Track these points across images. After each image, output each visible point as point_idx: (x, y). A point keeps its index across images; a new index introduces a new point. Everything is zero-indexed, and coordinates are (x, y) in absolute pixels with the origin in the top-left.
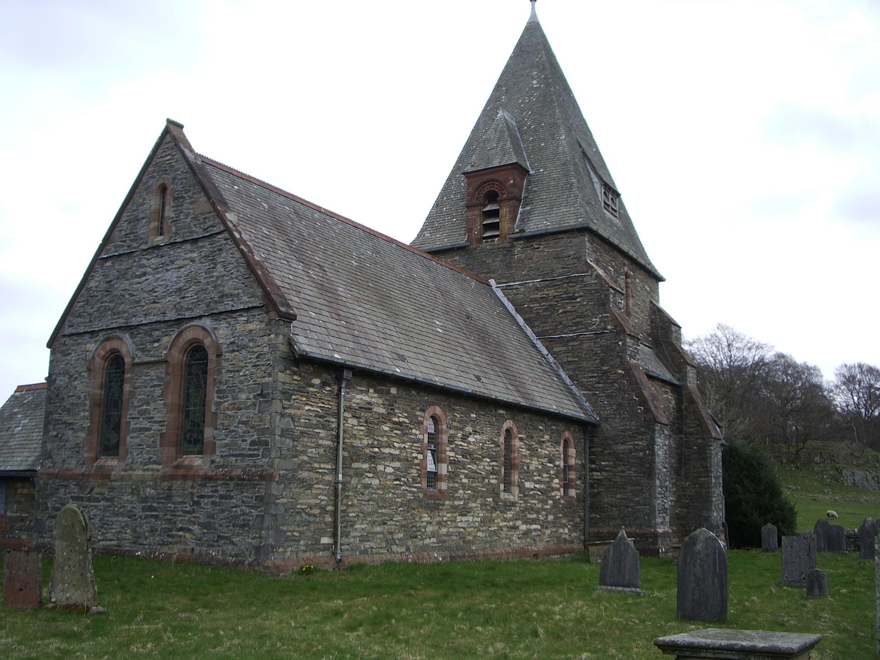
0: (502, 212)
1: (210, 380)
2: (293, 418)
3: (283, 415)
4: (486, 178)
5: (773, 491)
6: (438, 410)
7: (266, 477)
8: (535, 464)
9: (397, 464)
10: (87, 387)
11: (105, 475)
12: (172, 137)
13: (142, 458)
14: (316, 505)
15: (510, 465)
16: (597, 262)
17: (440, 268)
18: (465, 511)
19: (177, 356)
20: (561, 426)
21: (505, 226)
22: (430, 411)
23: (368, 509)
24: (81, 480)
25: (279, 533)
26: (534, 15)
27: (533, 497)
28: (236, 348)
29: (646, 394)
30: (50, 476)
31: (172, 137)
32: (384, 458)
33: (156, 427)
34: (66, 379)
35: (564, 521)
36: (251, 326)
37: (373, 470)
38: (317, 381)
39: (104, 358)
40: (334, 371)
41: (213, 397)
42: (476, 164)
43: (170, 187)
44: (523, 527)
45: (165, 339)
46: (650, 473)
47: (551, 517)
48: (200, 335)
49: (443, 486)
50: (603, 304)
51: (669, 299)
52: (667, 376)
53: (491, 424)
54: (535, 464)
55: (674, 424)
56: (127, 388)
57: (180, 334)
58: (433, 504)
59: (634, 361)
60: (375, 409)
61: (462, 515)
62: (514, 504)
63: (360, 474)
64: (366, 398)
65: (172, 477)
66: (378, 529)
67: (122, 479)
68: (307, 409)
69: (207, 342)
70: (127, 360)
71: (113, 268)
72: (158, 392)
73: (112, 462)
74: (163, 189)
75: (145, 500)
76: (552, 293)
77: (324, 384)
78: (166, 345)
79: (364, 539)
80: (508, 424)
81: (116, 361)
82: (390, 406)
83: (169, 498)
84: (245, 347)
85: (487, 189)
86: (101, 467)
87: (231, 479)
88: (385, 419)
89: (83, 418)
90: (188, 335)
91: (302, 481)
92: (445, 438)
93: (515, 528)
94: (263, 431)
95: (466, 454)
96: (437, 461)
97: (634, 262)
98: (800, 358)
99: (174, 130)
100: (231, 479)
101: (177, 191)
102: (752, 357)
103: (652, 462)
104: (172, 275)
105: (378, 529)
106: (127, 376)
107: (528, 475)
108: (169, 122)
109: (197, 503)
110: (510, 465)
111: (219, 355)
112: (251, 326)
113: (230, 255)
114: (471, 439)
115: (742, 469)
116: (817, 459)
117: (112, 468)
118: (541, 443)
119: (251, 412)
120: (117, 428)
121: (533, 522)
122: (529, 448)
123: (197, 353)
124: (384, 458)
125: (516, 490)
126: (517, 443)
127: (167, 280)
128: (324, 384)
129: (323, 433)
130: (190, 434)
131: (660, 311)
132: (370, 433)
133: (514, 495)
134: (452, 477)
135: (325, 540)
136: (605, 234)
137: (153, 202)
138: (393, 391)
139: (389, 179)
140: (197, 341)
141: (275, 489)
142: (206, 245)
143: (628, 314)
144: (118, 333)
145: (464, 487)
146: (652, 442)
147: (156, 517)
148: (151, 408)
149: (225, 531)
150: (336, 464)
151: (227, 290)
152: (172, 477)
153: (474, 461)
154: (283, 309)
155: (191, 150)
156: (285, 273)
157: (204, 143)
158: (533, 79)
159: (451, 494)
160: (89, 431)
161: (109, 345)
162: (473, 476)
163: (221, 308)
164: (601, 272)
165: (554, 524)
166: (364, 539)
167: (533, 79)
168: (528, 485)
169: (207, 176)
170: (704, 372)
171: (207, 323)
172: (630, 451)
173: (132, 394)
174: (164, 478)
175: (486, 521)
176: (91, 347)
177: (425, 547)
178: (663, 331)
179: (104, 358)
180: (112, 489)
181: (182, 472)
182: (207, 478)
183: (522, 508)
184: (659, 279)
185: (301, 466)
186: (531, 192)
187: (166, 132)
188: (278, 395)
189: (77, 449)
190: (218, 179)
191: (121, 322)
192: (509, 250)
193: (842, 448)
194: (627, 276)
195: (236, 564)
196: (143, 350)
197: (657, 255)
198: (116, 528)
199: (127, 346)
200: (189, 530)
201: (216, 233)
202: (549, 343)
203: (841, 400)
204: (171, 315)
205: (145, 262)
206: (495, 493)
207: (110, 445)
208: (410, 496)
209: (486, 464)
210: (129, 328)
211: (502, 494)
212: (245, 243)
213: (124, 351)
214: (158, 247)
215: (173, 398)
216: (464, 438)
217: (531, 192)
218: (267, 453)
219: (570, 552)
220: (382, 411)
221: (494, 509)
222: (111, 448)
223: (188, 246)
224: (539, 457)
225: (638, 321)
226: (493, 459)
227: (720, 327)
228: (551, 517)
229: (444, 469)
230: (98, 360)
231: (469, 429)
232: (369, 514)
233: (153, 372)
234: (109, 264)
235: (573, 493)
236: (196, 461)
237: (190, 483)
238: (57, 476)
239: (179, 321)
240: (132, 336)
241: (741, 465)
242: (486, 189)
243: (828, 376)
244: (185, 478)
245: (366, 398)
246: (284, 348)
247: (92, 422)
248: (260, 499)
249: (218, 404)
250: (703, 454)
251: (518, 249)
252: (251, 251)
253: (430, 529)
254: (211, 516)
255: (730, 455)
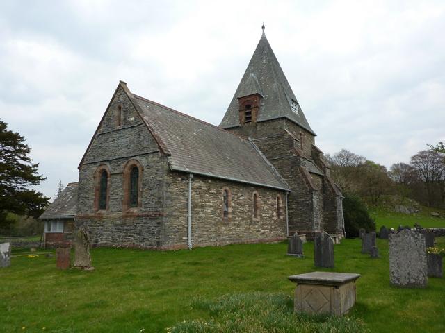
0: (252, 113)
1: (139, 179)
2: (171, 193)
3: (167, 192)
4: (246, 99)
5: (365, 214)
6: (227, 188)
7: (161, 215)
8: (266, 207)
9: (212, 209)
10: (94, 184)
11: (100, 217)
12: (122, 87)
13: (115, 211)
14: (180, 225)
15: (256, 208)
16: (289, 130)
17: (229, 134)
18: (239, 225)
19: (127, 171)
20: (276, 193)
21: (253, 118)
22: (224, 188)
23: (200, 225)
24: (91, 218)
25: (166, 236)
26: (264, 34)
27: (266, 219)
28: (149, 167)
29: (309, 179)
30: (80, 217)
31: (122, 87)
32: (206, 206)
33: (120, 198)
34: (85, 181)
35: (278, 228)
36: (154, 159)
37: (203, 211)
38: (180, 179)
39: (100, 172)
40: (184, 174)
41: (141, 185)
42: (242, 95)
43: (122, 107)
44: (263, 231)
45: (122, 165)
46: (312, 209)
47: (273, 227)
48: (136, 163)
49: (230, 216)
50: (291, 146)
51: (319, 143)
52: (319, 173)
53: (248, 193)
54: (266, 207)
55: (321, 190)
56: (109, 183)
57: (128, 162)
58: (226, 223)
59: (303, 167)
60: (203, 188)
61: (238, 227)
62: (258, 222)
63: (197, 213)
64: (199, 184)
65: (127, 216)
66: (205, 233)
67: (107, 218)
68: (176, 189)
69: (138, 165)
70: (109, 173)
71: (102, 138)
72: (120, 184)
73: (103, 211)
74: (120, 108)
75: (116, 225)
76: (272, 142)
77: (183, 179)
78: (123, 167)
79: (199, 237)
80: (255, 192)
81: (104, 173)
82: (209, 187)
83: (125, 224)
84: (152, 167)
85: (247, 104)
86: (99, 214)
87: (148, 216)
88: (207, 192)
89: (92, 195)
90: (131, 163)
91: (175, 216)
92: (230, 198)
93: (259, 231)
94: (159, 198)
95: (238, 204)
96: (227, 207)
97: (305, 130)
98: (376, 162)
99: (122, 85)
100: (148, 216)
101: (124, 108)
102: (356, 163)
103: (312, 205)
104: (124, 141)
105: (205, 233)
106: (109, 179)
107: (263, 211)
108: (120, 81)
109: (136, 226)
110: (256, 208)
111: (143, 170)
112: (154, 159)
113: (145, 132)
114: (241, 198)
115: (351, 206)
116: (384, 202)
117: (104, 214)
118: (268, 199)
119: (155, 191)
120: (105, 198)
121: (266, 229)
122: (264, 201)
123: (134, 169)
124: (206, 206)
125: (259, 217)
126: (258, 199)
127: (123, 143)
128: (183, 179)
129: (183, 198)
130: (133, 201)
131: (315, 147)
132: (201, 197)
133: (258, 219)
134: (234, 213)
135: (184, 238)
136: (292, 119)
137: (116, 113)
138: (210, 181)
139: (211, 103)
140: (134, 165)
141: (164, 219)
142: (137, 130)
143: (302, 149)
144: (105, 163)
145: (238, 216)
146: (312, 198)
147: (120, 232)
148: (118, 190)
149: (146, 236)
150: (188, 209)
151: (145, 146)
152: (127, 216)
153: (242, 206)
154: (166, 152)
155: (130, 93)
156: (168, 140)
157: (134, 89)
158: (264, 57)
159: (233, 219)
160: (95, 200)
161: (101, 168)
162: (242, 212)
163: (143, 153)
164: (290, 133)
165: (274, 229)
166: (199, 237)
167: (264, 57)
168: (263, 215)
169: (136, 102)
170: (334, 167)
171: (138, 158)
172: (303, 201)
173: (111, 186)
174: (123, 217)
175: (247, 229)
176: (95, 168)
177: (224, 240)
178: (316, 154)
179: (100, 172)
180: (103, 222)
181: (129, 214)
182: (139, 216)
183: (262, 223)
184: (314, 135)
185: (174, 211)
186: (263, 100)
187: (120, 86)
188: (165, 184)
189: (90, 207)
190: (140, 104)
191: (106, 159)
192: (256, 127)
193: (394, 198)
194: (301, 134)
195: (150, 249)
196: (114, 169)
197: (313, 125)
198: (105, 237)
199: (108, 167)
200: (132, 236)
201: (140, 124)
202: (271, 160)
203: (394, 178)
204: (125, 156)
205: (114, 136)
206: (250, 218)
207: (103, 206)
208: (217, 220)
209: (247, 207)
210: (108, 161)
211: (254, 219)
212: (151, 128)
213: (107, 169)
214: (118, 130)
215: (126, 186)
216: (238, 198)
217: (263, 100)
218: (162, 206)
219: (282, 240)
220: (206, 189)
221: (251, 224)
222: (103, 206)
223: (130, 129)
224: (267, 204)
225: (306, 152)
226: (250, 205)
227: (344, 151)
228: (273, 227)
229: (230, 210)
230: (97, 173)
231: (239, 194)
232: (202, 227)
233: (118, 177)
234: (100, 137)
235: (281, 217)
236: (135, 210)
237: (133, 219)
238: (83, 217)
239: (127, 158)
240: (110, 164)
241: (353, 204)
242: (246, 104)
243: (389, 169)
244: (131, 216)
245: (199, 184)
246: (166, 167)
247: (95, 196)
248: (159, 223)
249: (142, 188)
250: (333, 202)
251: (258, 126)
252: (153, 130)
253: (225, 232)
254: (140, 231)
255: (347, 202)
